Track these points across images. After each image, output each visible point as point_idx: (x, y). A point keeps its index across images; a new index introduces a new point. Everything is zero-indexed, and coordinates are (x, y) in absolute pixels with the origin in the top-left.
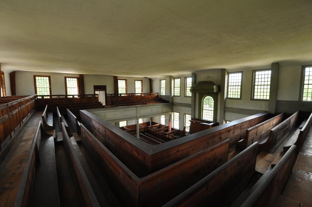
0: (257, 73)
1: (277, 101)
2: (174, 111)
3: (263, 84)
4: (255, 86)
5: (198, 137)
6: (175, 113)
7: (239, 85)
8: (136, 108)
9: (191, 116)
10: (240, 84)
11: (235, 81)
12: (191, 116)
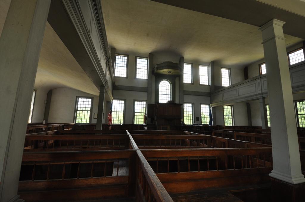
0: (80, 99)
1: (215, 86)
2: (209, 87)
3: (84, 112)
4: (78, 111)
5: (268, 23)
6: (207, 84)
7: (88, 110)
8: (263, 92)
9: (88, 122)
10: (89, 109)
11: (84, 106)
12: (88, 122)
